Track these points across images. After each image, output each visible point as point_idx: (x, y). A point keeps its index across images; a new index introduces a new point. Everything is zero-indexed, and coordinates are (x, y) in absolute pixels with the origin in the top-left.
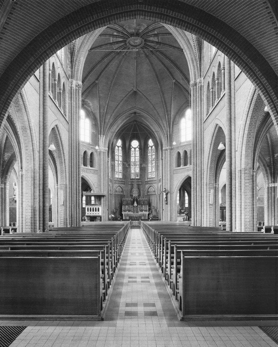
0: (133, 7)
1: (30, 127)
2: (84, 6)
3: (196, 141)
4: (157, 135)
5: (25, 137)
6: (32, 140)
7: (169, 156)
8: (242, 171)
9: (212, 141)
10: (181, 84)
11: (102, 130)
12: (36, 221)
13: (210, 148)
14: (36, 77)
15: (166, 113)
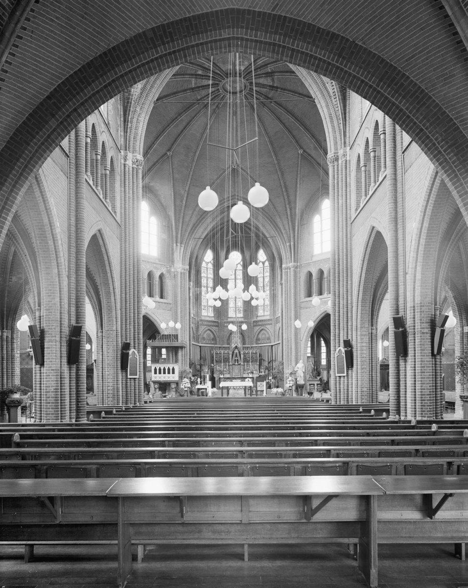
0: (225, 32)
1: (53, 235)
2: (141, 31)
3: (339, 256)
4: (271, 243)
5: (44, 251)
6: (57, 257)
7: (292, 278)
8: (416, 308)
9: (365, 255)
10: (312, 157)
11: (179, 236)
12: (65, 395)
13: (362, 268)
14: (62, 149)
15: (287, 206)
